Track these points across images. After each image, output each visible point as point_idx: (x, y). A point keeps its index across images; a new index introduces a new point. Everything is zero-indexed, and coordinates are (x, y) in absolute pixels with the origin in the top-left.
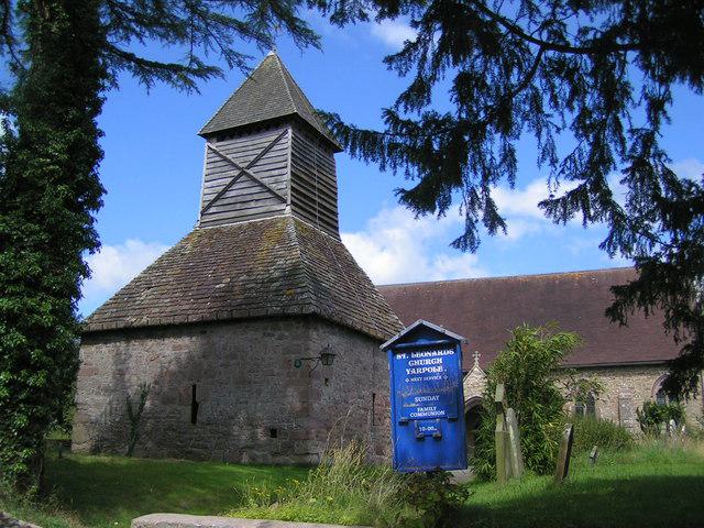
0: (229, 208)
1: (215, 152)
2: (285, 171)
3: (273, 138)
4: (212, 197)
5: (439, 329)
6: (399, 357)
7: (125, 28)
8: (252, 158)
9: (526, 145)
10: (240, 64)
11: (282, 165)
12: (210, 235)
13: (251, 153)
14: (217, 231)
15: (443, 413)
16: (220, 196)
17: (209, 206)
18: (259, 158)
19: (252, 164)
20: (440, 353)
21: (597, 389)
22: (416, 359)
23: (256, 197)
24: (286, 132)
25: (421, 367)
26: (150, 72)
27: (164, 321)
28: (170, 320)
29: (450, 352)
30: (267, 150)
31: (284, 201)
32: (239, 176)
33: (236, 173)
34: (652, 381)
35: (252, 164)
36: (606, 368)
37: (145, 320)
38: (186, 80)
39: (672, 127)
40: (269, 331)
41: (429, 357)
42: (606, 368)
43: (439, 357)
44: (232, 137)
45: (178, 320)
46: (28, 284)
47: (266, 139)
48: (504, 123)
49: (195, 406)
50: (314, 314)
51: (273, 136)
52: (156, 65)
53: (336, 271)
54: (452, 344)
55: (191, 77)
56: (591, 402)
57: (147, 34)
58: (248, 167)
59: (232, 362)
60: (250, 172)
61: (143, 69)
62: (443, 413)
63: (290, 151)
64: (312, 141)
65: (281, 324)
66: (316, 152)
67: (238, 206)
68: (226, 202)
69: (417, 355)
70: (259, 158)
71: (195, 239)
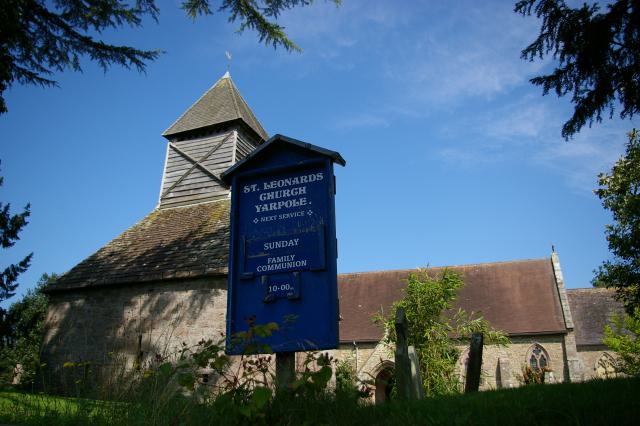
1: (175, 150)
6: (247, 189)
7: (83, 17)
11: (229, 159)
12: (166, 215)
14: (171, 212)
15: (304, 263)
19: (204, 159)
20: (304, 179)
22: (270, 191)
23: (206, 185)
24: (232, 134)
25: (276, 200)
26: (106, 56)
27: (118, 281)
30: (218, 148)
34: (525, 349)
35: (204, 159)
38: (138, 63)
39: (586, 1)
40: (205, 289)
41: (290, 187)
43: (301, 185)
44: (190, 138)
51: (220, 138)
52: (112, 49)
55: (140, 58)
58: (202, 161)
60: (202, 165)
62: (304, 263)
63: (235, 148)
65: (217, 283)
67: (192, 192)
68: (181, 189)
69: (272, 185)
71: (155, 218)
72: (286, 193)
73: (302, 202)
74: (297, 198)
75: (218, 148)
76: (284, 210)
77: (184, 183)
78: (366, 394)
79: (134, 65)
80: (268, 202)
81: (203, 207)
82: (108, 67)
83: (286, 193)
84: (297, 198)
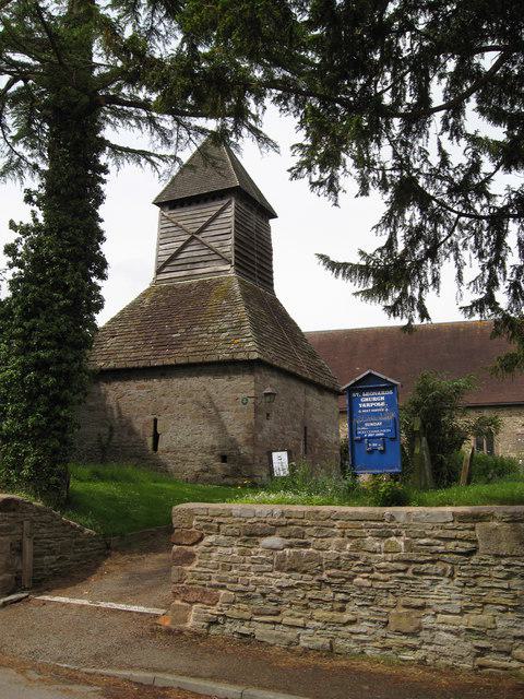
0: (180, 268)
2: (229, 237)
3: (219, 208)
4: (167, 258)
5: (384, 377)
6: (354, 395)
8: (201, 225)
9: (447, 268)
10: (213, 165)
13: (199, 220)
16: (173, 257)
17: (164, 266)
18: (207, 225)
19: (201, 231)
21: (495, 423)
23: (204, 258)
24: (230, 203)
26: (121, 154)
27: (130, 365)
28: (135, 364)
29: (391, 393)
30: (214, 218)
31: (230, 263)
32: (189, 241)
33: (187, 237)
35: (201, 231)
36: (504, 406)
37: (112, 364)
38: (153, 163)
42: (504, 406)
45: (142, 364)
46: (58, 340)
47: (215, 207)
48: (432, 254)
49: (156, 437)
50: (258, 361)
52: (127, 150)
53: (273, 323)
54: (392, 387)
56: (490, 436)
57: (120, 124)
59: (188, 400)
60: (200, 237)
61: (116, 153)
63: (232, 219)
64: (251, 209)
66: (254, 217)
68: (177, 262)
70: (207, 225)
72: (374, 399)
73: (383, 404)
74: (381, 402)
75: (214, 218)
76: (374, 407)
77: (182, 256)
78: (413, 140)
79: (149, 164)
80: (366, 402)
81: (203, 284)
82: (122, 166)
83: (374, 399)
84: (381, 402)
